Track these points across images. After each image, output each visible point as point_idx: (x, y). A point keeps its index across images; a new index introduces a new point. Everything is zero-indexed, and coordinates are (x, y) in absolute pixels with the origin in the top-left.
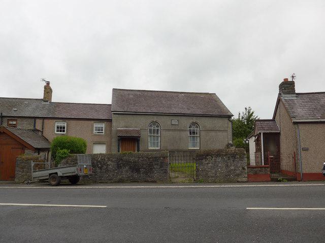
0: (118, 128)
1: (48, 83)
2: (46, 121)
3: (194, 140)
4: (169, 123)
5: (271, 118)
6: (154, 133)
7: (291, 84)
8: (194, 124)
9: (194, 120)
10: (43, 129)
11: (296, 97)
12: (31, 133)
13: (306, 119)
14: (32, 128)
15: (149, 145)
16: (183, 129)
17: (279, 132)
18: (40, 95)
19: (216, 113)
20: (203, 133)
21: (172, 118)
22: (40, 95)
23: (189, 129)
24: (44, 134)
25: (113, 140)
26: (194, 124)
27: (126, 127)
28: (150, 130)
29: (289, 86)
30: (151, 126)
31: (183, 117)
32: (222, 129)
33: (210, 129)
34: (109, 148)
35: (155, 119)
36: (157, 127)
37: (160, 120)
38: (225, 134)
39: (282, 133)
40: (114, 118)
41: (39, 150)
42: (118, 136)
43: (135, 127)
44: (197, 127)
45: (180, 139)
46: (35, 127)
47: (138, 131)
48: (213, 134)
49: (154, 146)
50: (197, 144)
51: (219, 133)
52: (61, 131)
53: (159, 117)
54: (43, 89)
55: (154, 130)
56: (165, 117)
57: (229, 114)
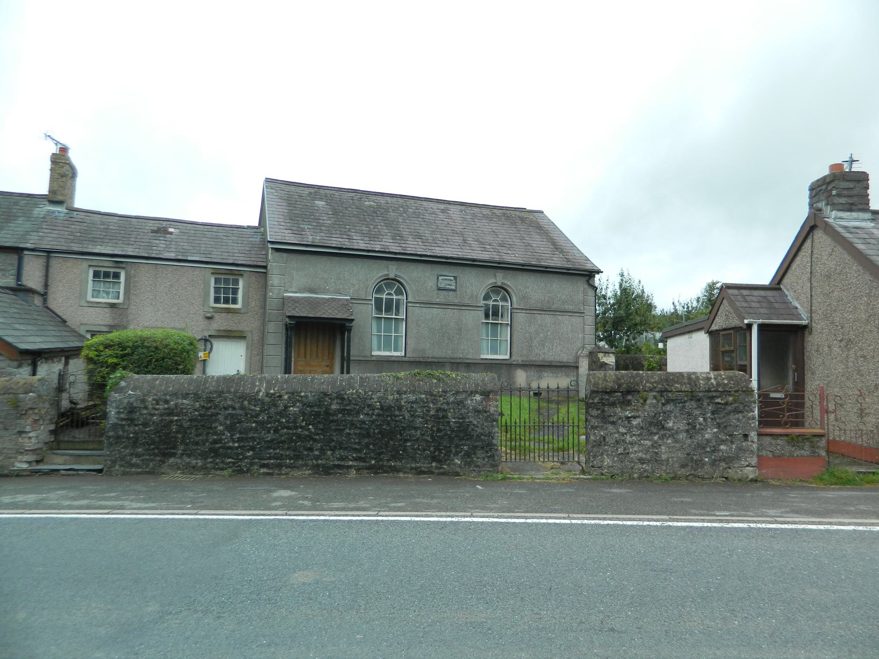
0: (287, 291)
1: (64, 150)
4: (431, 283)
5: (765, 279)
6: (388, 309)
7: (859, 181)
8: (497, 289)
9: (500, 279)
10: (46, 286)
11: (873, 220)
12: (8, 298)
14: (11, 281)
16: (467, 301)
17: (804, 322)
18: (40, 185)
19: (556, 261)
20: (520, 317)
21: (439, 270)
22: (40, 185)
23: (482, 303)
24: (52, 305)
25: (271, 327)
26: (497, 289)
28: (378, 301)
29: (851, 185)
30: (379, 290)
31: (468, 270)
32: (571, 308)
33: (539, 305)
34: (257, 359)
35: (393, 270)
37: (410, 275)
38: (576, 320)
39: (817, 327)
40: (275, 262)
41: (34, 357)
42: (289, 317)
44: (504, 299)
45: (460, 329)
46: (19, 276)
47: (346, 305)
48: (548, 319)
49: (387, 347)
50: (503, 344)
51: (565, 319)
53: (405, 265)
54: (48, 165)
55: (389, 302)
56: (421, 267)
57: (589, 267)
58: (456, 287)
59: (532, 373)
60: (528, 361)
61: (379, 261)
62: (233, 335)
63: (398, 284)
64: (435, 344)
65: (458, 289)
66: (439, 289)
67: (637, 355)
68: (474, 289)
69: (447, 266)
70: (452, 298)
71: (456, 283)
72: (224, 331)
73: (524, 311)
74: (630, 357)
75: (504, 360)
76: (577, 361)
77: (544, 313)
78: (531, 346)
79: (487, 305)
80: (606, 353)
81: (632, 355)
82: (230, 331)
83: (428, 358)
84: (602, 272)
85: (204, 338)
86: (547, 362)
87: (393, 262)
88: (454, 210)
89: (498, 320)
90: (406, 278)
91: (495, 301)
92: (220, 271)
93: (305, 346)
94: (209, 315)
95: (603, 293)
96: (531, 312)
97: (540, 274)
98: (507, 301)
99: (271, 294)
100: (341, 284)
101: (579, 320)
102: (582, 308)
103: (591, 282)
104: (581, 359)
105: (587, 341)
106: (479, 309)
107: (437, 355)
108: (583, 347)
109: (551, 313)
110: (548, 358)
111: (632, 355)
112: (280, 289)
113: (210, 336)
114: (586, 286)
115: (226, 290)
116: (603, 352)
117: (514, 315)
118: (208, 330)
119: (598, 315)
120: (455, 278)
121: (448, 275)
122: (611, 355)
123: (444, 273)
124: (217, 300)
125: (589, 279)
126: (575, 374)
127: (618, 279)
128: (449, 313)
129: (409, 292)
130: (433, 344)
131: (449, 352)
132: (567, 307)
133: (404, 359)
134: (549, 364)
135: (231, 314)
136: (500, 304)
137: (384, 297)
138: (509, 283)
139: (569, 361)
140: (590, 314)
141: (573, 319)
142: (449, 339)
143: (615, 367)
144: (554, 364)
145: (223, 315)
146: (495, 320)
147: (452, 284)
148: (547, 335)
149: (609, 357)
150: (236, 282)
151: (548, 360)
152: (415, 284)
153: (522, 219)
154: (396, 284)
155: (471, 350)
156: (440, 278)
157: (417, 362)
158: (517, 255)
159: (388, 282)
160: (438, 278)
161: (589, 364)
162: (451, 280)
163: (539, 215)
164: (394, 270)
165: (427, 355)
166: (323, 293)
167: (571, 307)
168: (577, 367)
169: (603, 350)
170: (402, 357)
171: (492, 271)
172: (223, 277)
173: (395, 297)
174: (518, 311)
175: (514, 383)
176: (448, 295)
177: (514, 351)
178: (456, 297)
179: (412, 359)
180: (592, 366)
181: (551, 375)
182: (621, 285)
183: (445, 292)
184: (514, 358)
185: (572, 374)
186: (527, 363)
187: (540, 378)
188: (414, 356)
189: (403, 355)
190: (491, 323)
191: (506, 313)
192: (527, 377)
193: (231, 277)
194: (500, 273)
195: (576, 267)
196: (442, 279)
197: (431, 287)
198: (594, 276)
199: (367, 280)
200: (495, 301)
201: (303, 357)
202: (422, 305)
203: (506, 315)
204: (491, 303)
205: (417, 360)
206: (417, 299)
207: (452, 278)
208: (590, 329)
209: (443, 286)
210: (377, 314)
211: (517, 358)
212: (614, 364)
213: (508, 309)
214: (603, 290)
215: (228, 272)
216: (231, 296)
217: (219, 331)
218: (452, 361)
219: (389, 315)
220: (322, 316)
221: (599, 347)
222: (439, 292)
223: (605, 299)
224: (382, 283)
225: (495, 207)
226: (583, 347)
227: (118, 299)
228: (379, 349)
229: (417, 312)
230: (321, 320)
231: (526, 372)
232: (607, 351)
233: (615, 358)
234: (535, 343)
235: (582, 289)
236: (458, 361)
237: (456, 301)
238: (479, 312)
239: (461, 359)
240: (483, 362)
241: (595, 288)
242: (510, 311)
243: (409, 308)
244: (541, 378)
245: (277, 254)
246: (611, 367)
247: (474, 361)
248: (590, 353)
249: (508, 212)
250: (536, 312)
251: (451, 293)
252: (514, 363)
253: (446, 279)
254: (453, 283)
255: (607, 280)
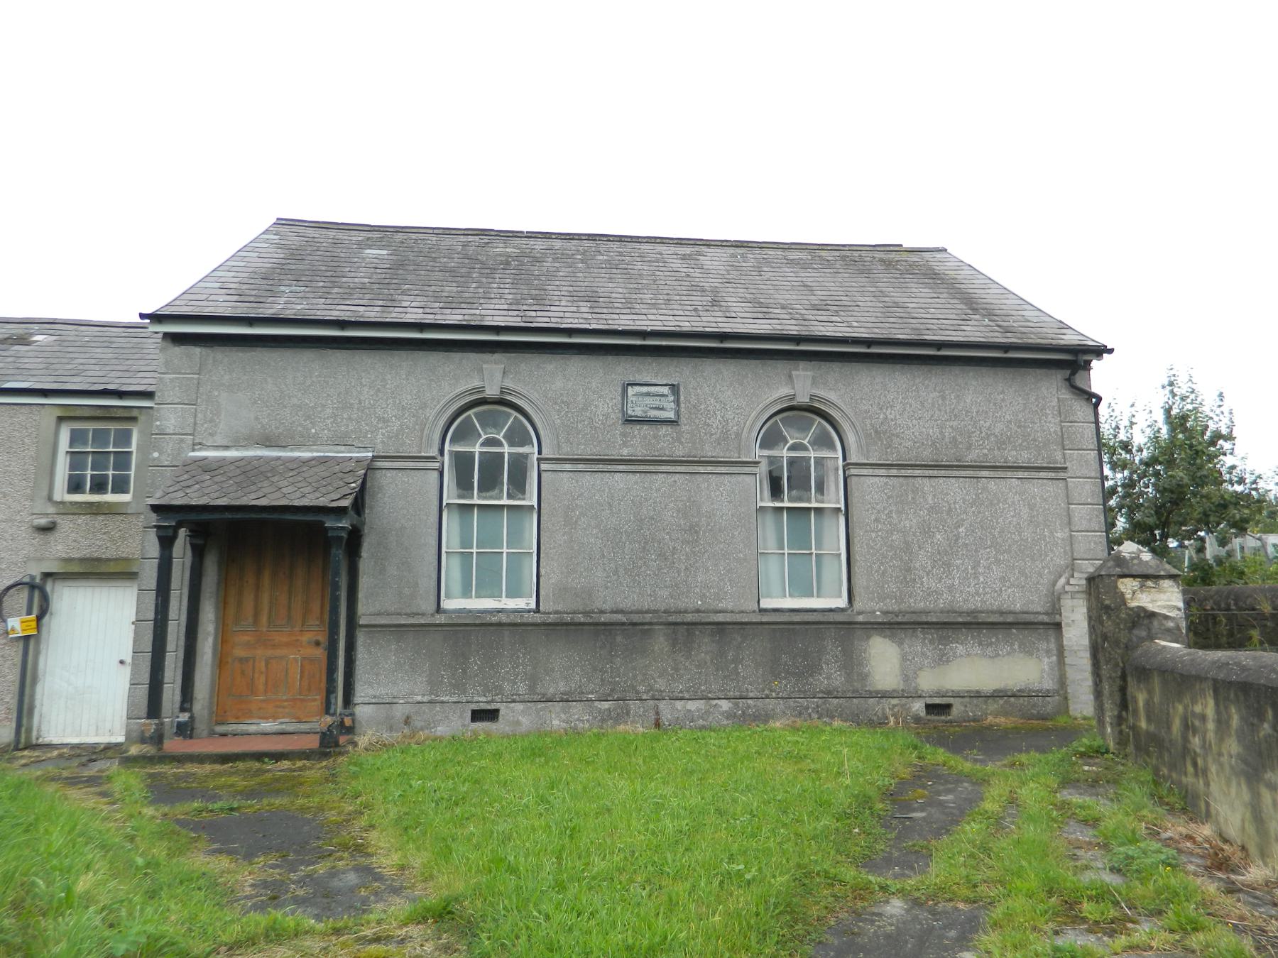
0: (202, 446)
2: (436, 474)
3: (800, 539)
4: (606, 406)
6: (490, 482)
13: (447, 542)
15: (452, 571)
16: (709, 452)
19: (974, 331)
20: (871, 488)
21: (625, 369)
27: (268, 442)
28: (463, 463)
31: (709, 367)
32: (1024, 457)
33: (927, 455)
36: (518, 437)
38: (1042, 490)
42: (156, 508)
43: (342, 441)
44: (823, 441)
45: (693, 529)
48: (955, 490)
49: (488, 586)
50: (828, 565)
51: (1008, 489)
52: (99, 486)
55: (492, 466)
56: (576, 364)
57: (1069, 339)
58: (678, 413)
59: (919, 645)
60: (904, 613)
61: (457, 356)
62: (103, 569)
63: (515, 414)
64: (621, 571)
65: (683, 420)
66: (629, 421)
67: (1233, 586)
68: (730, 415)
69: (649, 359)
70: (664, 442)
71: (677, 402)
72: (83, 560)
73: (882, 472)
74: (1217, 592)
75: (831, 610)
76: (1055, 609)
77: (943, 473)
78: (908, 570)
79: (772, 460)
80: (1146, 577)
81: (1219, 586)
82: (98, 560)
83: (602, 612)
84: (1111, 351)
85: (27, 580)
86: (960, 613)
87: (497, 356)
88: (715, 260)
89: (809, 501)
90: (534, 396)
91: (794, 448)
92: (78, 413)
93: (258, 588)
94: (43, 521)
95: (1122, 436)
96: (903, 472)
97: (925, 368)
98: (831, 446)
99: (156, 455)
100: (350, 418)
101: (1053, 489)
102: (1059, 456)
103: (1079, 381)
104: (1067, 603)
105: (1080, 549)
106: (747, 470)
107: (626, 604)
108: (1072, 568)
109: (963, 473)
110: (965, 601)
111: (1219, 586)
112: (182, 440)
113: (47, 575)
114: (1066, 395)
115: (100, 459)
116: (1134, 576)
117: (853, 482)
118: (40, 560)
119: (1113, 491)
120: (674, 388)
121: (654, 381)
122: (1166, 583)
123: (640, 378)
124: (75, 485)
125: (1073, 374)
126: (1053, 646)
127: (1161, 398)
128: (661, 482)
129: (542, 433)
130: (616, 572)
131: (664, 593)
132: (1012, 455)
133: (538, 618)
134: (968, 619)
135: (101, 518)
136: (812, 454)
137: (477, 449)
138: (832, 396)
139: (1032, 608)
140: (1085, 472)
141: (1034, 489)
142: (662, 556)
143: (1183, 624)
144: (982, 617)
145: (81, 520)
146: (800, 499)
147: (666, 405)
148: (957, 537)
149: (1161, 590)
150: (125, 438)
151: (965, 608)
152: (559, 411)
153: (888, 264)
154: (509, 415)
155: (728, 588)
156: (631, 391)
157: (567, 624)
158: (855, 324)
159: (490, 411)
160: (624, 391)
161: (1090, 618)
162: (663, 395)
163: (938, 255)
164: (499, 375)
165: (598, 604)
166: (299, 446)
167: (1025, 455)
168: (1058, 626)
169: (1136, 570)
170: (529, 611)
171: (781, 366)
172: (90, 426)
173: (506, 449)
174: (865, 472)
175: (864, 677)
176: (655, 437)
177: (860, 581)
178: (679, 440)
179: (552, 618)
180: (1101, 623)
181: (977, 650)
182: (1168, 411)
183: (645, 427)
184: (858, 605)
185: (1044, 645)
186: (900, 619)
187: (943, 660)
188: (560, 608)
189: (533, 606)
190: (788, 509)
191: (832, 478)
192: (904, 658)
193: (112, 426)
194: (805, 369)
195: (1030, 341)
196: (636, 395)
197: (607, 416)
198: (1087, 366)
199: (424, 406)
200: (794, 448)
201: (251, 620)
202: (581, 467)
203: (832, 488)
204: (784, 453)
205: (568, 618)
206: (566, 451)
207: (666, 390)
208: (1087, 515)
209: (638, 412)
210: (460, 497)
211: (870, 605)
212: (1181, 614)
213: (837, 469)
214: (1122, 431)
215: (98, 413)
216: (110, 473)
217: (69, 560)
218: (672, 619)
219: (491, 498)
220: (296, 503)
221: (1120, 561)
222: (628, 429)
223: (1130, 452)
224: (471, 412)
225: (822, 247)
226: (1072, 568)
227: (532, 553)
228: (466, 593)
229: (563, 483)
230: (228, 516)
231: (900, 643)
232: (1151, 572)
233: (1184, 592)
234: (922, 559)
235: (1055, 402)
236: (689, 618)
237: (679, 452)
238: (748, 479)
239: (698, 611)
240: (765, 619)
241: (1094, 400)
242: (841, 472)
243: (544, 475)
244: (948, 661)
245: (178, 351)
246: (1171, 624)
247: (738, 618)
248: (1091, 580)
249: (856, 254)
250: (917, 472)
251: (664, 430)
252: (860, 618)
253: (648, 394)
254: (669, 403)
255: (1132, 405)
